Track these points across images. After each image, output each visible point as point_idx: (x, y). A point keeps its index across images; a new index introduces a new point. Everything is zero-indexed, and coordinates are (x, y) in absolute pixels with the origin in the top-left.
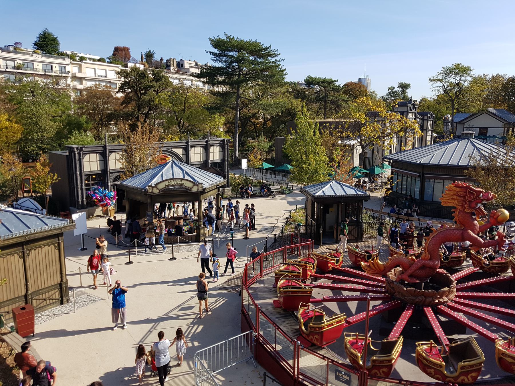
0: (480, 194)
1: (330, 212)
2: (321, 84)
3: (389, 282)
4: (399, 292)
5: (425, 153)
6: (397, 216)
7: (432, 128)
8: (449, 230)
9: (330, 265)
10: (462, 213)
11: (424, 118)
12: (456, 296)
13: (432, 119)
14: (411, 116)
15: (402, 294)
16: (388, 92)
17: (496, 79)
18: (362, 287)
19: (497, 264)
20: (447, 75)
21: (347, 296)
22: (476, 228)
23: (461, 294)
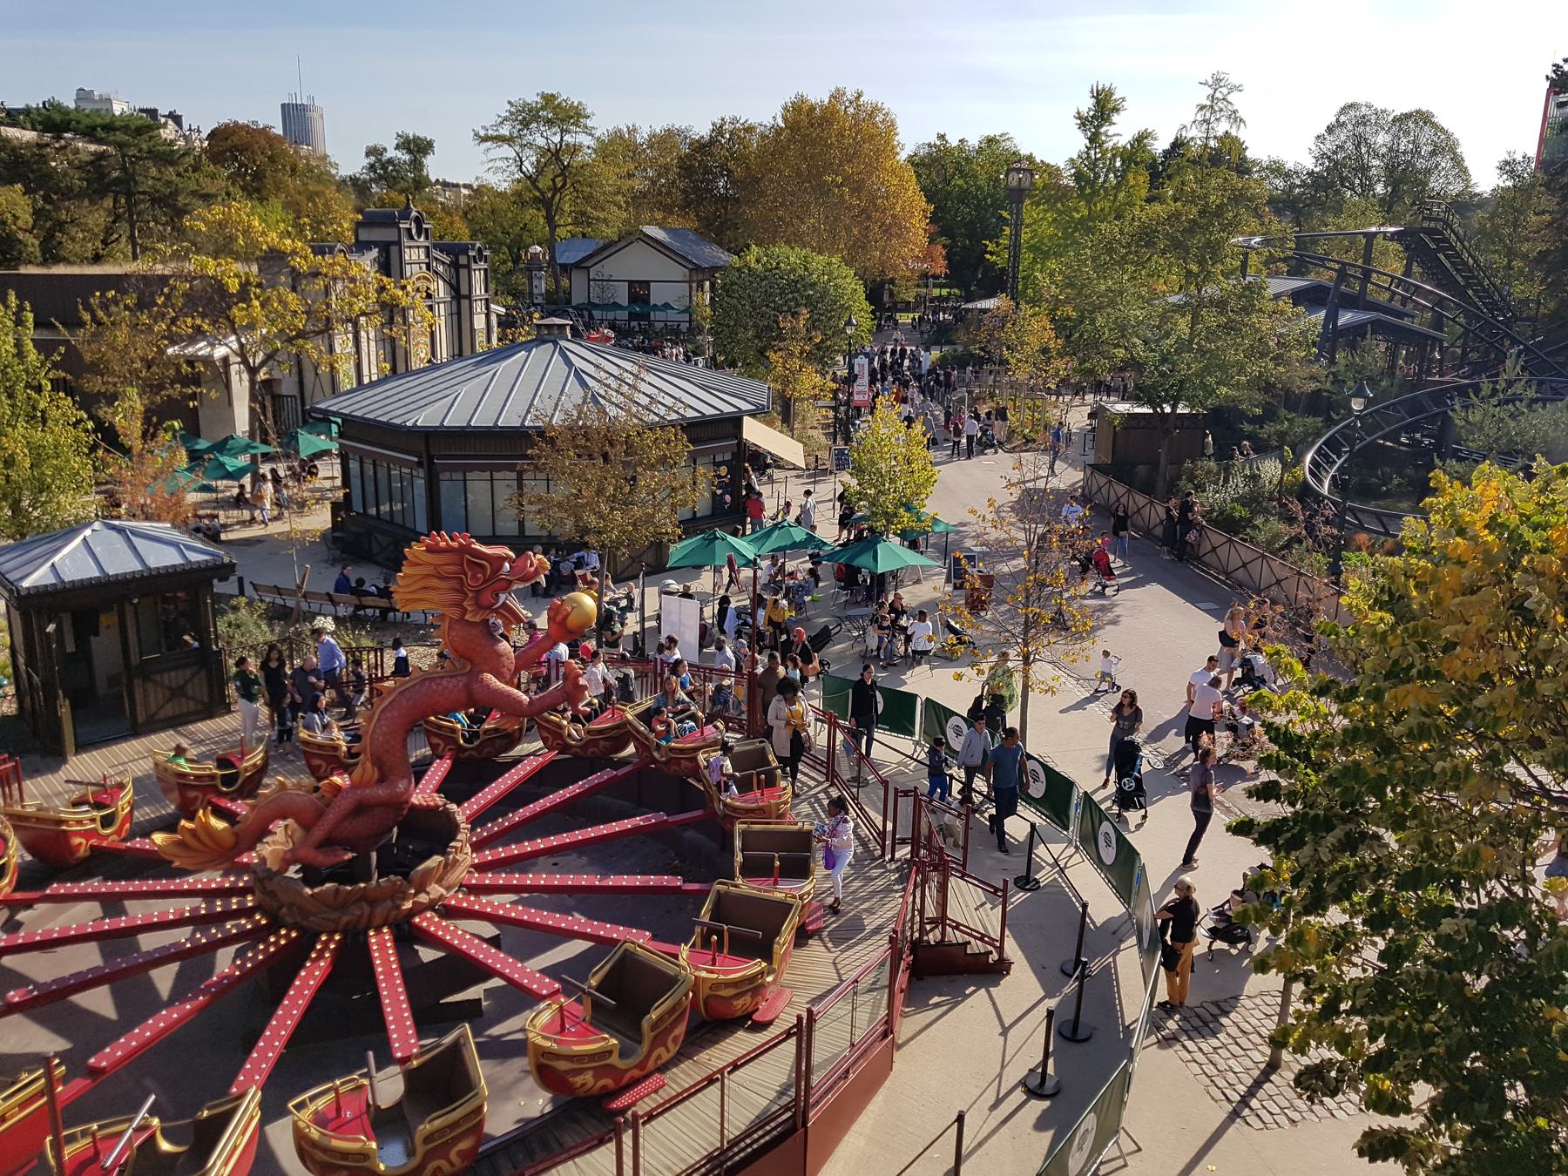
0: (501, 566)
1: (102, 629)
2: (100, 133)
3: (264, 878)
4: (291, 905)
5: (434, 390)
6: (357, 602)
7: (486, 291)
8: (427, 683)
9: (77, 840)
10: (457, 627)
11: (457, 260)
12: (481, 868)
13: (483, 265)
14: (414, 257)
15: (300, 909)
16: (366, 162)
17: (665, 140)
18: (187, 906)
19: (600, 731)
20: (525, 124)
21: (89, 971)
22: (506, 662)
23: (488, 855)
